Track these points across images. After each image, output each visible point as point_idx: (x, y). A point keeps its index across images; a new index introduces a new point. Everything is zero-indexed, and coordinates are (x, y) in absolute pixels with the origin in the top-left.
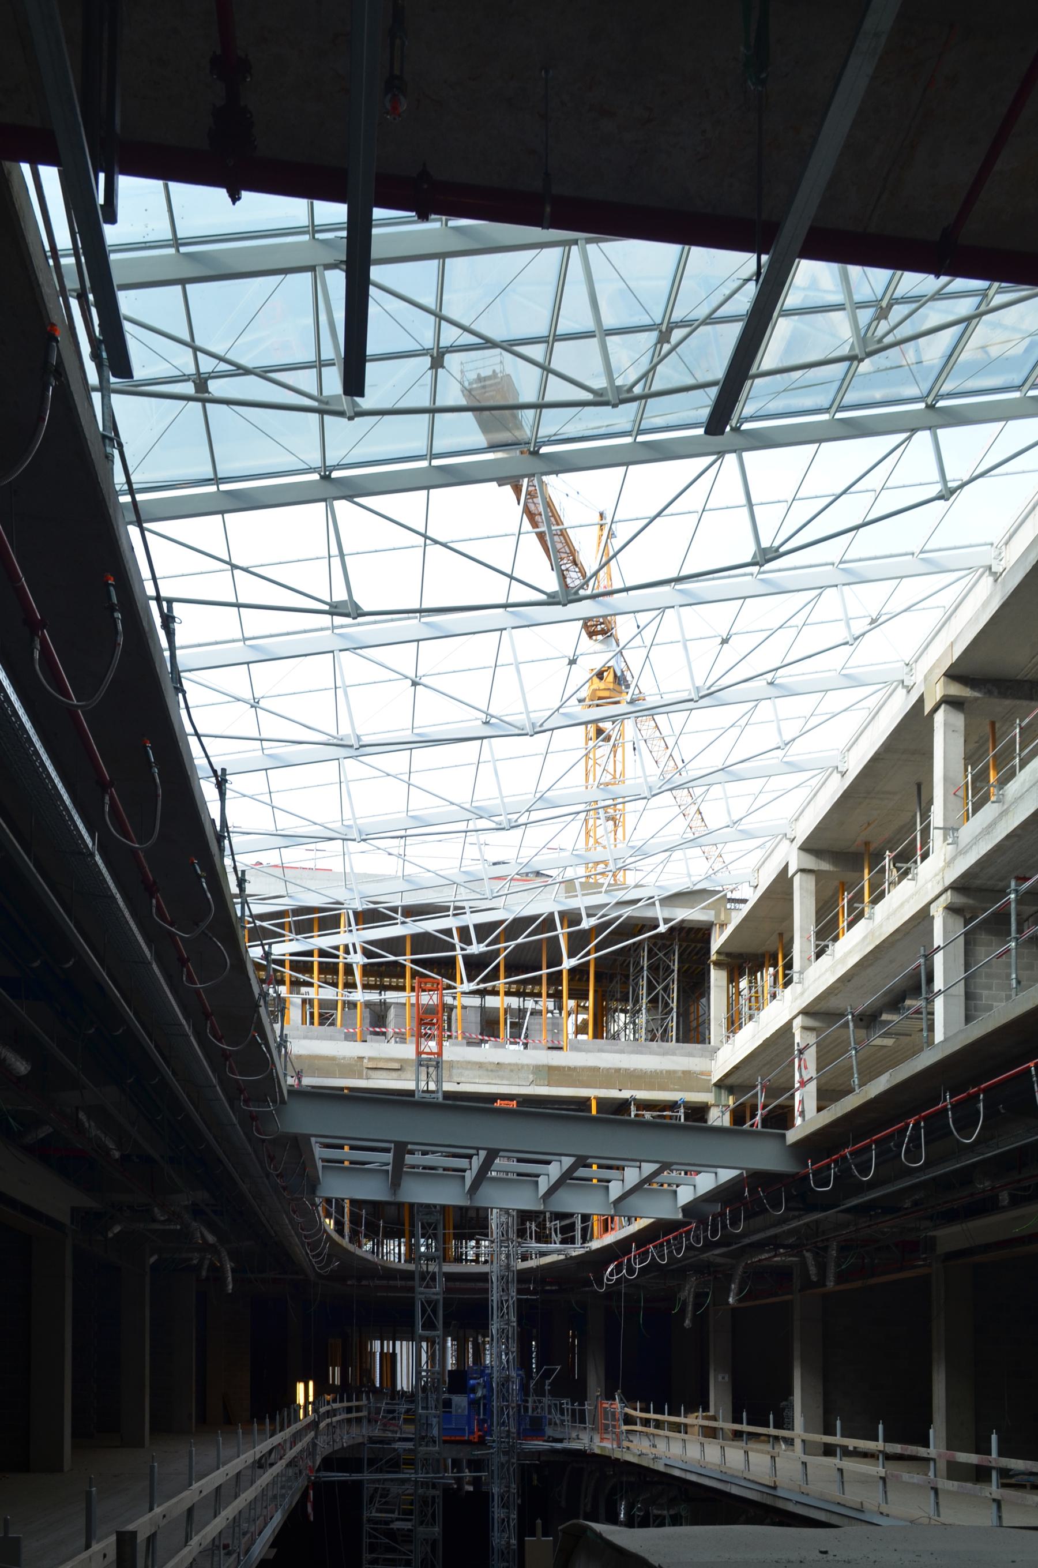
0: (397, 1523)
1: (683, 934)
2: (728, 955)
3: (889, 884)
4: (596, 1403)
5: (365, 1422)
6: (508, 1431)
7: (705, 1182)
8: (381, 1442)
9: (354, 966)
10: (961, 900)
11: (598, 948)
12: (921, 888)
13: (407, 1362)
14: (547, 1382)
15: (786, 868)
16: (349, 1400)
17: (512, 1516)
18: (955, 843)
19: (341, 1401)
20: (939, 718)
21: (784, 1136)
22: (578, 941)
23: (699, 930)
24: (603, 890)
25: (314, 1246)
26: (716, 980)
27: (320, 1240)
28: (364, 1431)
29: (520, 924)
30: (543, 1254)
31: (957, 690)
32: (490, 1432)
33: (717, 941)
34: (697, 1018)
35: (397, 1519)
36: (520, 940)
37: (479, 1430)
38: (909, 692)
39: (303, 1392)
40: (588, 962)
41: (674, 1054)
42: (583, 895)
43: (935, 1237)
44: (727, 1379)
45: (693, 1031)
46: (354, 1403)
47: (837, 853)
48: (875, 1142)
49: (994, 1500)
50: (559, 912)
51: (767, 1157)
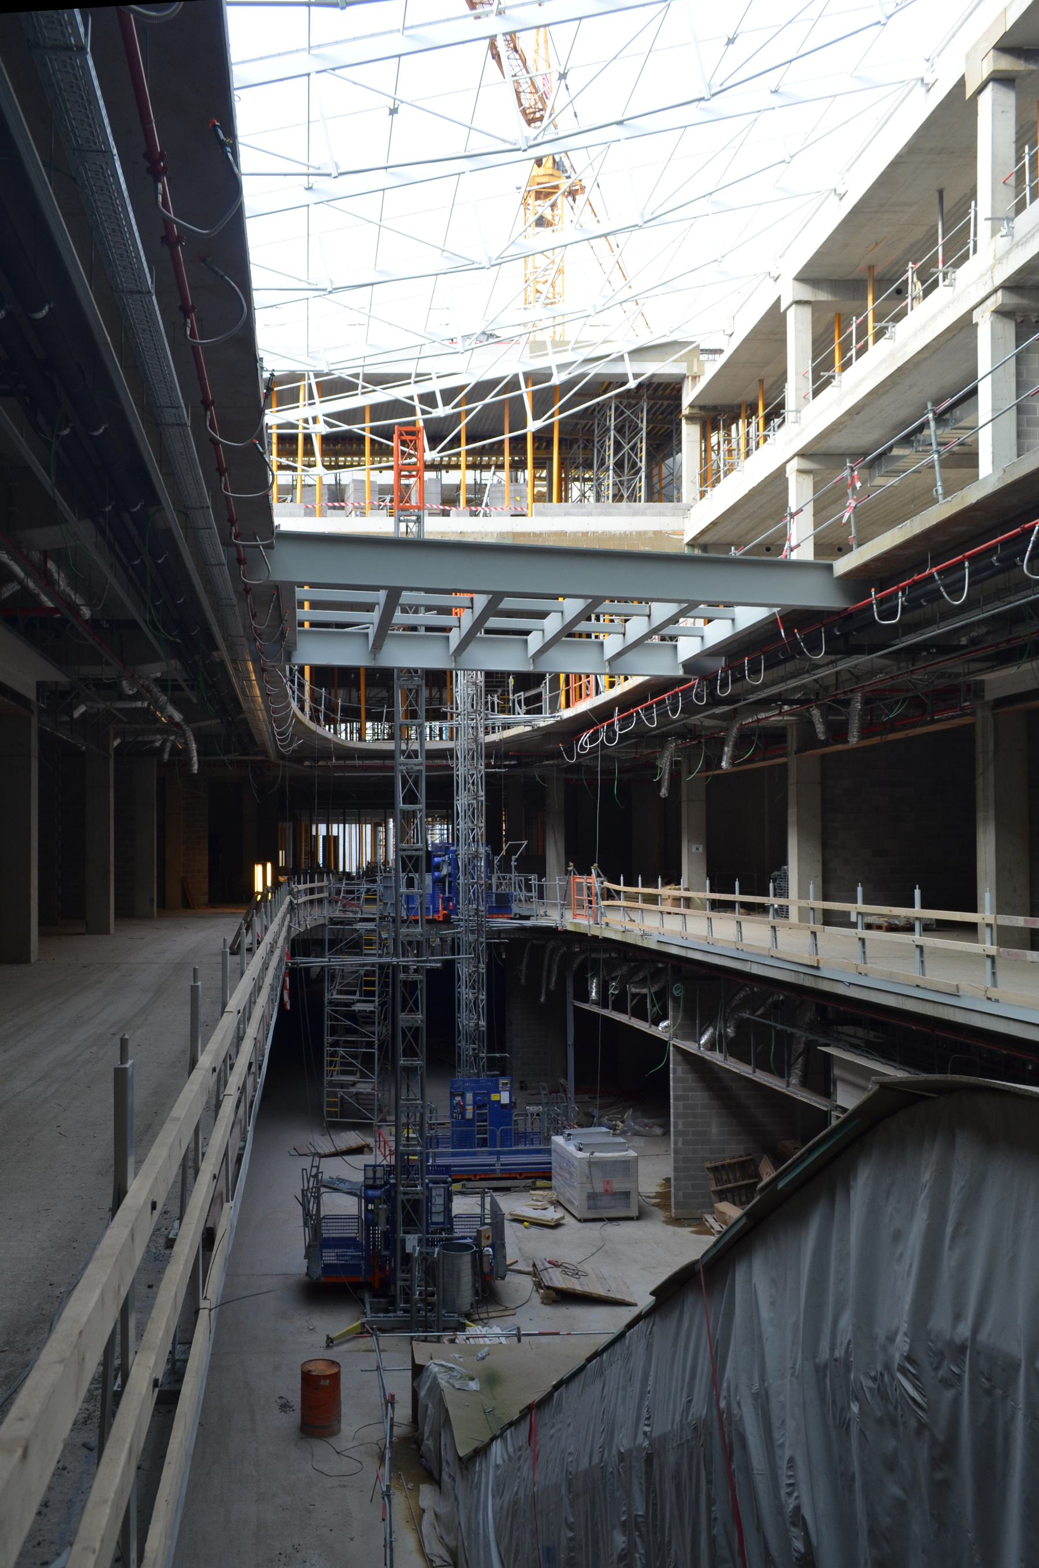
0: (358, 1005)
1: (650, 392)
2: (702, 408)
3: (913, 299)
4: (554, 880)
5: (326, 902)
6: (477, 909)
7: (718, 632)
8: (341, 923)
9: (313, 436)
10: (1013, 300)
11: (562, 410)
12: (970, 287)
13: (355, 844)
14: (514, 858)
15: (778, 300)
16: (312, 881)
17: (481, 997)
18: (1010, 234)
19: (305, 883)
20: (986, 102)
21: (830, 567)
22: (543, 402)
23: (668, 385)
24: (570, 347)
25: (280, 722)
26: (688, 435)
27: (287, 716)
28: (325, 913)
29: (482, 388)
30: (506, 726)
31: (1007, 64)
32: (455, 911)
33: (689, 396)
34: (660, 480)
35: (359, 1001)
36: (488, 400)
37: (444, 909)
38: (928, 91)
39: (261, 876)
40: (552, 424)
41: (644, 514)
42: (554, 353)
43: (982, 681)
44: (701, 850)
45: (662, 490)
46: (316, 884)
47: (836, 281)
48: (969, 558)
49: (988, 956)
50: (524, 374)
51: (816, 595)
